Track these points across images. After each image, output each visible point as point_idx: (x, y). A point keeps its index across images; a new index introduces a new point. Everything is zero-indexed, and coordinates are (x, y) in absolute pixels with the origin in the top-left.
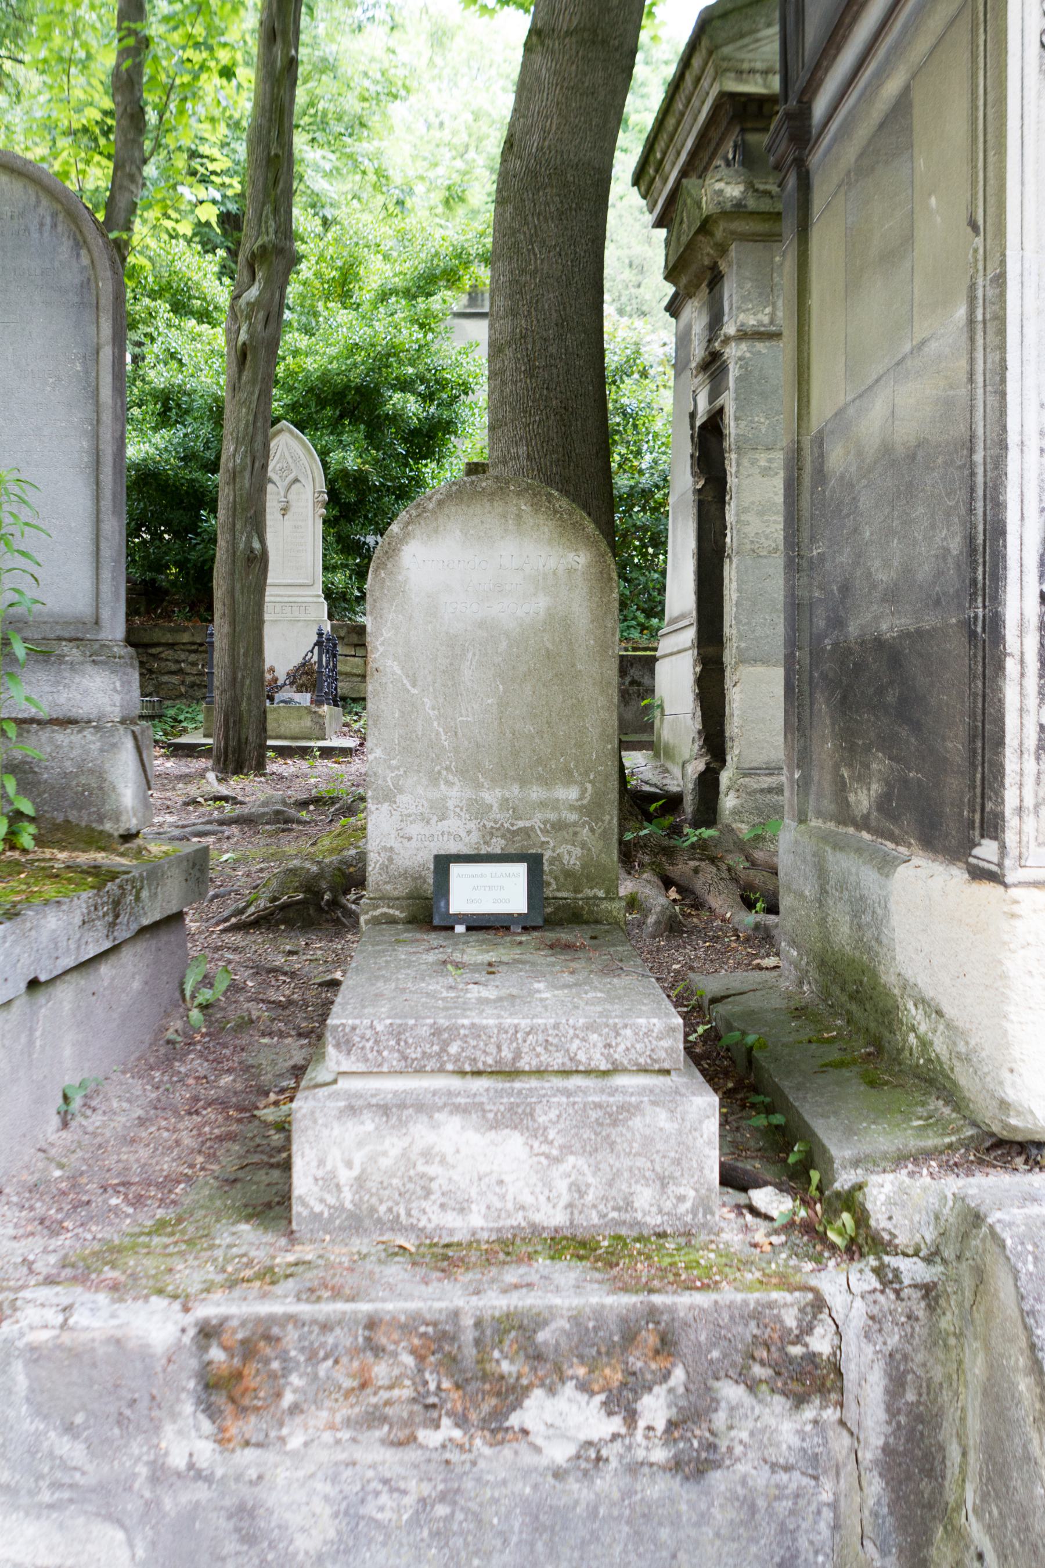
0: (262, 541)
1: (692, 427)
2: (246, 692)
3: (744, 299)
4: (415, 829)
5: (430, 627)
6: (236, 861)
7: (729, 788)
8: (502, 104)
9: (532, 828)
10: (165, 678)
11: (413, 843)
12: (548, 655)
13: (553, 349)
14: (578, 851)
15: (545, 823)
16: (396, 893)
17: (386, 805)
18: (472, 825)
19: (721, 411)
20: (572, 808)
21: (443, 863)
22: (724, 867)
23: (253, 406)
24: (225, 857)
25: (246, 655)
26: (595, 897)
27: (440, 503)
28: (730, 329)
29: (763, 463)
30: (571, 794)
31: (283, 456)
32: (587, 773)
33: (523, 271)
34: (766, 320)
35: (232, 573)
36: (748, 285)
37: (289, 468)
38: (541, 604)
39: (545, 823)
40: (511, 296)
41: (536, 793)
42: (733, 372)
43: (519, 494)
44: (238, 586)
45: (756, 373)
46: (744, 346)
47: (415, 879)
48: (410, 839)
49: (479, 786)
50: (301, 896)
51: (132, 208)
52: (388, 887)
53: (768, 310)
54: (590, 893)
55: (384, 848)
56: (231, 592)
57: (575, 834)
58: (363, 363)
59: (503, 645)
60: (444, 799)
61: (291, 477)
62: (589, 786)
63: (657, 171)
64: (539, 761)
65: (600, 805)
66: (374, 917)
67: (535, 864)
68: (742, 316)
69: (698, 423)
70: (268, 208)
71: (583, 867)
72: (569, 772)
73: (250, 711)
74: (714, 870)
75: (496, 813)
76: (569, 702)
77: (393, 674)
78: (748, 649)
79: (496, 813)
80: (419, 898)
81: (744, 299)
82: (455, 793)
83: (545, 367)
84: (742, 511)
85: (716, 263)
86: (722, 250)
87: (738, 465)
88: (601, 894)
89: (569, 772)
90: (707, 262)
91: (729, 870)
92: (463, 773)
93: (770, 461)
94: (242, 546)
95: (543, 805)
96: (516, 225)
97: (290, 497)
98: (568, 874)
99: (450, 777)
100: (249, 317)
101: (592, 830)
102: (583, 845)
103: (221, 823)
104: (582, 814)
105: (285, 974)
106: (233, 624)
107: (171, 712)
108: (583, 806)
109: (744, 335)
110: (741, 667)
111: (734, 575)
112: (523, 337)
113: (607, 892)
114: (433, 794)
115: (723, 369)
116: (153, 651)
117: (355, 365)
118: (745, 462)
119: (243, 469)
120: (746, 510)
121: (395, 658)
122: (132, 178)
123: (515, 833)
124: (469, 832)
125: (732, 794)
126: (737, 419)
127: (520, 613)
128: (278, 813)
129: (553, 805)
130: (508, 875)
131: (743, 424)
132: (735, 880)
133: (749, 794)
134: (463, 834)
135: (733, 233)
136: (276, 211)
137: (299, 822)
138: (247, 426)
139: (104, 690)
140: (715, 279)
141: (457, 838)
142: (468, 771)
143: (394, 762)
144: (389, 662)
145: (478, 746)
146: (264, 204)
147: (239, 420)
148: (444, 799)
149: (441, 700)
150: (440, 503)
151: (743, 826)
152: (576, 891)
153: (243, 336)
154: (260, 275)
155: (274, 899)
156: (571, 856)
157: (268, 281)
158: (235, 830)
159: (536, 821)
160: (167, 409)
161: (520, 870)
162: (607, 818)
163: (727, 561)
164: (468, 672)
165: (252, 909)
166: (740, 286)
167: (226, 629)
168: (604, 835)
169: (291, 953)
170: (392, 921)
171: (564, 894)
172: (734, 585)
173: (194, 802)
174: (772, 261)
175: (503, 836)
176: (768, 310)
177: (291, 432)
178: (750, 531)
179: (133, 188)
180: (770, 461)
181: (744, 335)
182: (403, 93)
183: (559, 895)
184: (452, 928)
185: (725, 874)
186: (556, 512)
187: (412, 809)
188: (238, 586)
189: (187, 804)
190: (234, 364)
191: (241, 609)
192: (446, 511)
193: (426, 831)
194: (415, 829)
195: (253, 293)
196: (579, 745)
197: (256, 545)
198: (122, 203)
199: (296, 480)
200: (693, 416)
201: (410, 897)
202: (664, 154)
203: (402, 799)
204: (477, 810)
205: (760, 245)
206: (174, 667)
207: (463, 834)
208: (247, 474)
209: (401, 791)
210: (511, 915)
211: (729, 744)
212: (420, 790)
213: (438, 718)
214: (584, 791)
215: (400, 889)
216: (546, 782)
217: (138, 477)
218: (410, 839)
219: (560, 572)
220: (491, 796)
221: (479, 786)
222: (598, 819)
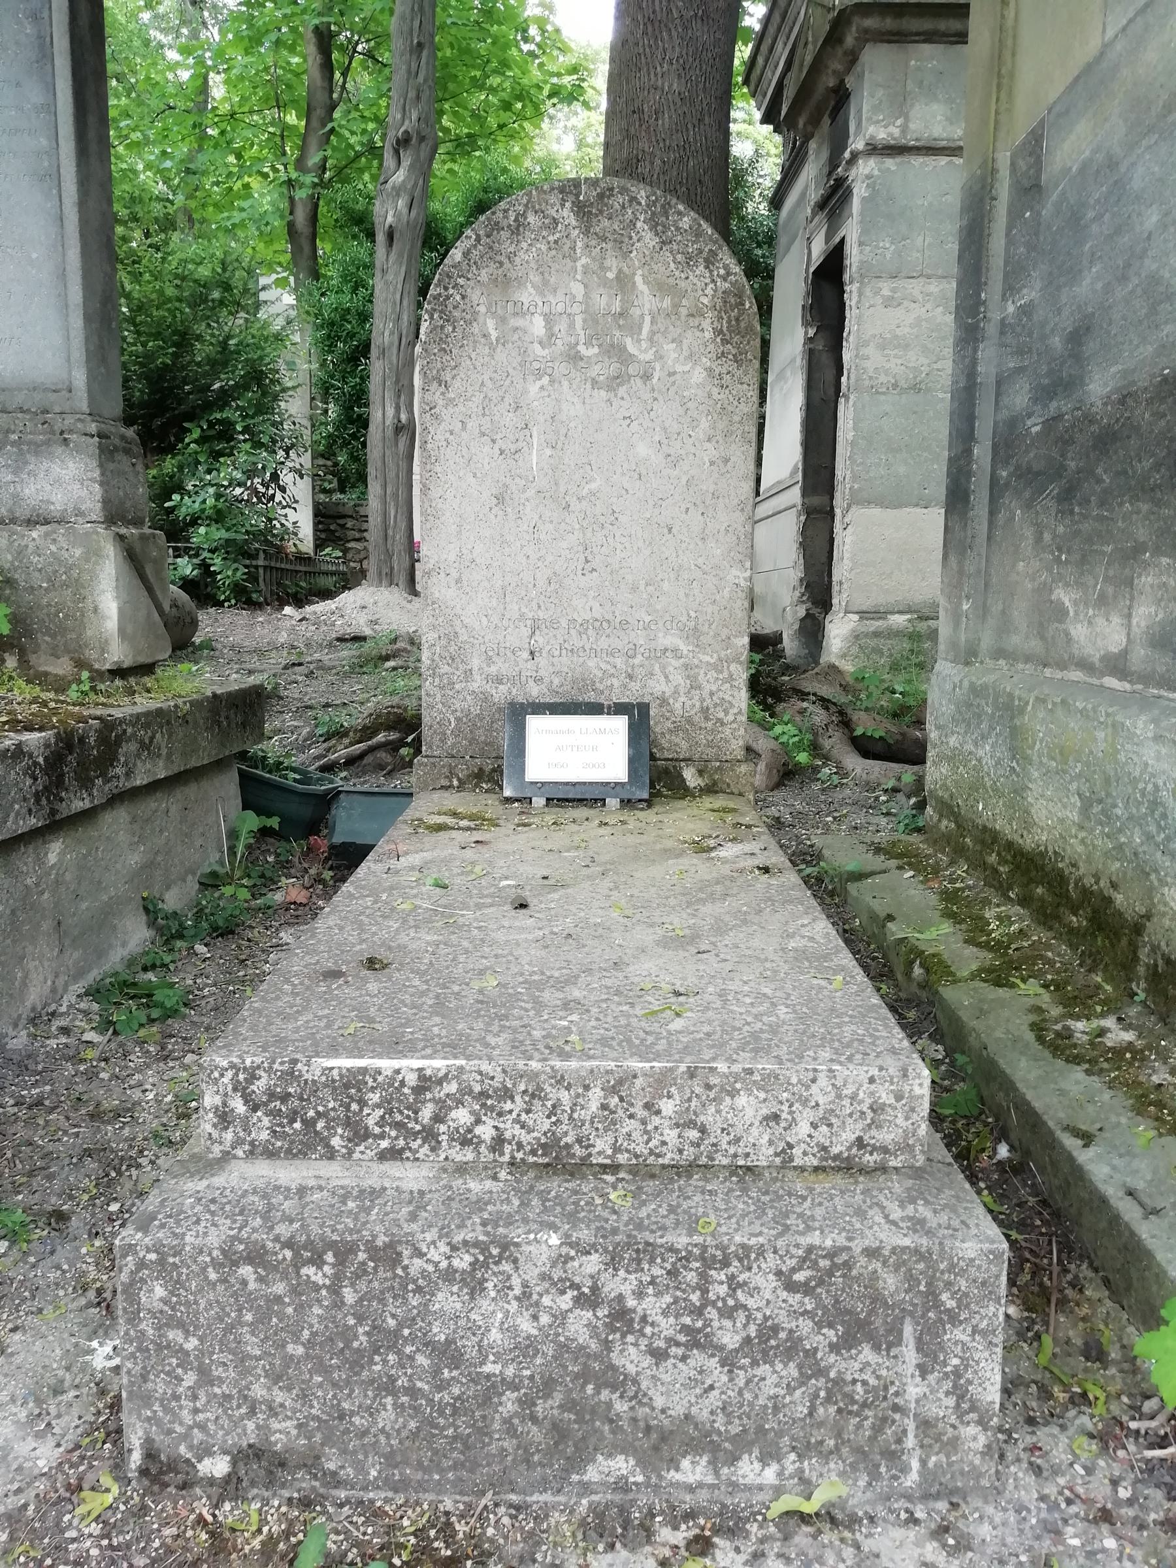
3: (876, 109)
28: (857, 144)
29: (886, 292)
34: (896, 132)
42: (859, 192)
53: (899, 122)
67: (639, 717)
68: (872, 130)
81: (876, 109)
86: (853, 59)
87: (860, 295)
90: (832, 82)
109: (875, 150)
116: (341, 522)
118: (868, 292)
120: (866, 344)
126: (861, 244)
130: (602, 732)
135: (866, 31)
139: (69, 481)
161: (619, 725)
163: (842, 400)
174: (907, 65)
176: (899, 122)
178: (869, 365)
180: (894, 290)
181: (875, 150)
197: (404, 417)
211: (835, 588)
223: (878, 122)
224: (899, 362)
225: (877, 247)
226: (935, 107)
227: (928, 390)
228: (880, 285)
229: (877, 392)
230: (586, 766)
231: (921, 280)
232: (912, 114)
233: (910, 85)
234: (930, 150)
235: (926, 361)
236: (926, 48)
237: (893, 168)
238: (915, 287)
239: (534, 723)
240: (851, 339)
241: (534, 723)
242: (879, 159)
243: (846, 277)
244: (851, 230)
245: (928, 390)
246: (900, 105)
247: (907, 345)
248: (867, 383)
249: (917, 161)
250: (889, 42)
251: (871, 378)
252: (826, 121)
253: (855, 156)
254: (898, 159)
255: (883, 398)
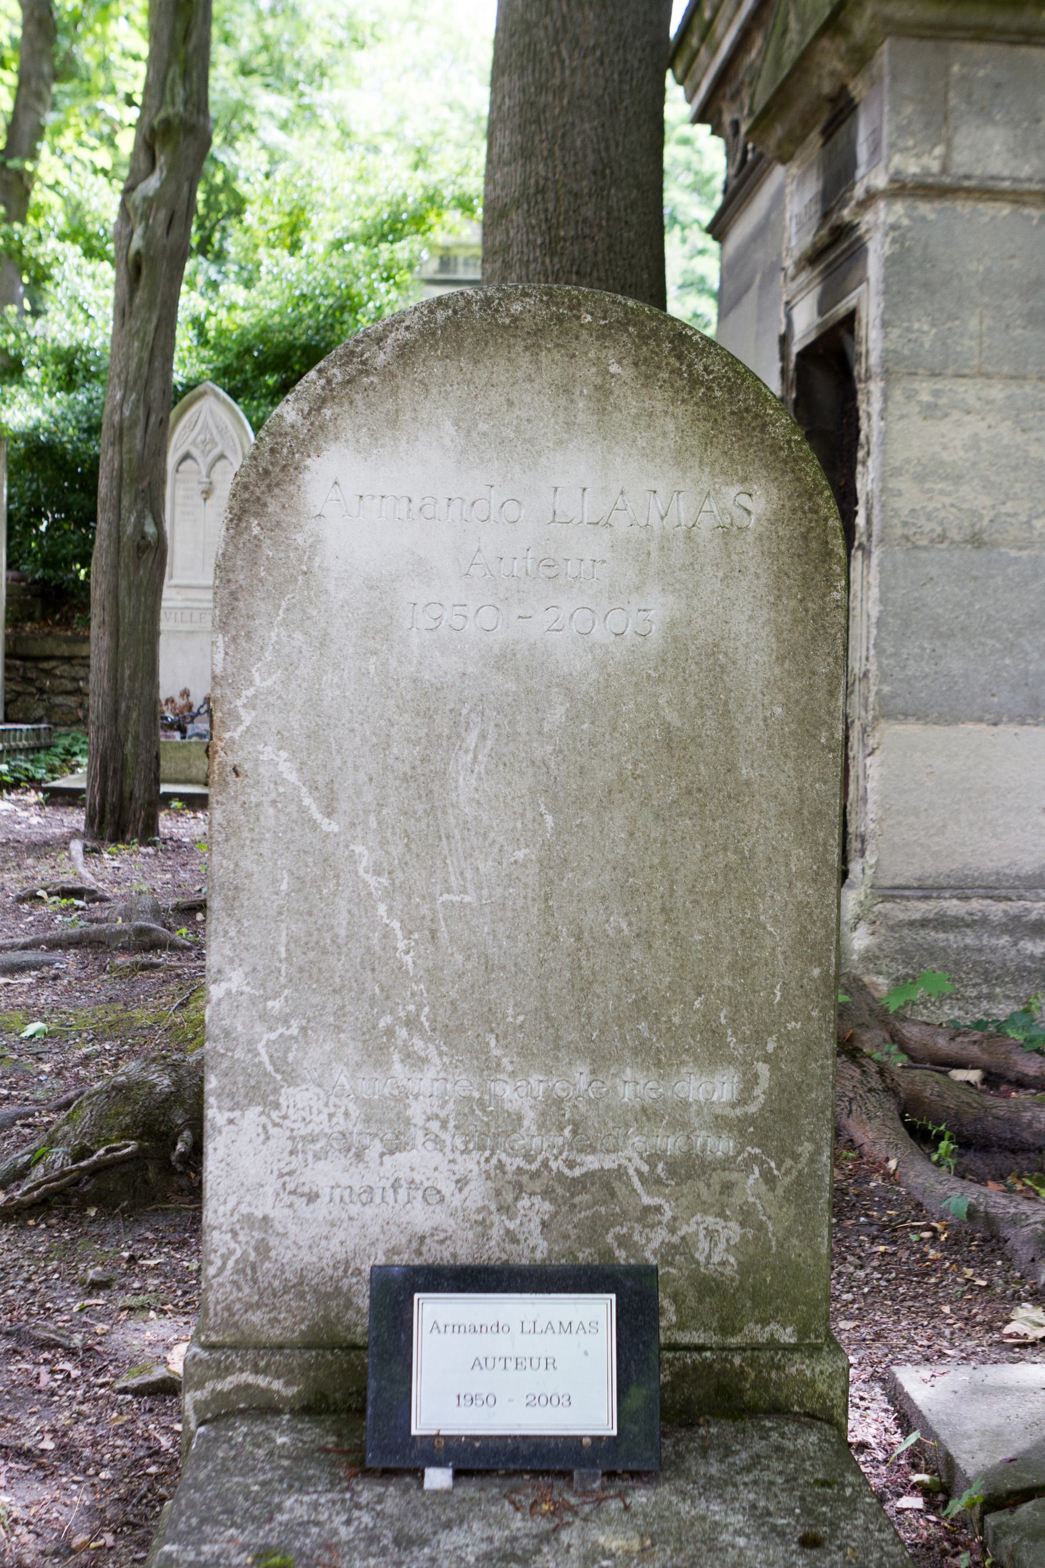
0: (159, 523)
1: (784, 356)
2: (132, 729)
3: (902, 131)
4: (325, 1174)
5: (372, 665)
6: (49, 1035)
7: (859, 919)
8: (478, 98)
9: (620, 1172)
10: (59, 700)
11: (321, 1209)
12: (669, 740)
13: (588, 211)
14: (733, 1231)
15: (652, 1160)
16: (275, 1334)
17: (253, 1113)
18: (471, 1165)
19: (850, 319)
20: (720, 1124)
21: (397, 1291)
22: (873, 1068)
23: (149, 338)
24: (31, 1029)
25: (133, 678)
26: (773, 1344)
27: (405, 353)
29: (925, 397)
30: (720, 1088)
31: (205, 426)
32: (758, 1037)
33: (542, 88)
34: (935, 166)
35: (116, 566)
36: (908, 109)
37: (213, 441)
38: (653, 612)
39: (652, 1160)
40: (522, 128)
41: (632, 1086)
42: (877, 252)
43: (603, 335)
44: (123, 584)
45: (918, 253)
46: (899, 208)
47: (323, 1298)
48: (312, 1197)
49: (488, 1067)
50: (132, 1146)
51: (39, 132)
52: (256, 1317)
53: (939, 151)
54: (761, 1334)
55: (249, 1221)
56: (114, 592)
57: (727, 1187)
58: (310, 316)
59: (558, 714)
60: (402, 1097)
61: (216, 452)
62: (763, 1069)
63: (702, 40)
64: (641, 1007)
65: (788, 1118)
66: (219, 1397)
67: (638, 1300)
68: (897, 160)
69: (796, 348)
70: (175, 71)
71: (744, 1269)
72: (713, 1035)
73: (136, 755)
74: (857, 1073)
75: (530, 1136)
76: (719, 861)
77: (278, 780)
78: (894, 695)
79: (530, 1136)
80: (332, 1346)
81: (902, 131)
82: (429, 1085)
83: (574, 239)
84: (889, 473)
85: (843, 89)
86: (861, 58)
87: (886, 398)
88: (787, 1336)
89: (713, 1035)
90: (827, 88)
91: (881, 1072)
92: (447, 1033)
93: (936, 393)
94: (129, 529)
95: (648, 1115)
96: (532, 16)
97: (214, 476)
98: (707, 1287)
99: (418, 1044)
100: (145, 217)
101: (769, 1179)
102: (746, 1216)
103: (54, 945)
104: (743, 1138)
105: (71, 1353)
106: (115, 635)
107: (65, 742)
108: (747, 1120)
109: (902, 189)
110: (883, 725)
111: (874, 577)
112: (541, 191)
113: (803, 1332)
114: (375, 1086)
115: (857, 251)
116: (45, 665)
117: (300, 319)
118: (897, 394)
119: (134, 424)
120: (896, 472)
121: (284, 740)
122: (39, 96)
123: (579, 1185)
124: (462, 1183)
125: (863, 929)
126: (885, 324)
127: (601, 634)
128: (141, 931)
129: (676, 1116)
131: (895, 333)
132: (891, 1090)
133: (892, 928)
134: (447, 1188)
135: (887, 21)
136: (186, 75)
137: (174, 947)
138: (140, 366)
140: (840, 112)
141: (433, 1196)
142: (463, 1030)
143: (275, 1005)
144: (268, 752)
145: (488, 967)
146: (169, 65)
147: (129, 358)
148: (402, 1097)
149: (397, 850)
150: (405, 353)
151: (881, 980)
152: (727, 1328)
153: (137, 243)
154: (161, 160)
155: (82, 1153)
156: (716, 1243)
157: (173, 168)
158: (68, 961)
159: (630, 1155)
160: (71, 371)
161: (598, 1311)
162: (806, 1148)
164: (466, 783)
165: (38, 1172)
166: (896, 110)
167: (106, 642)
168: (799, 1192)
169: (97, 1286)
170: (265, 1408)
171: (697, 1338)
172: (875, 592)
173: (33, 897)
175: (547, 1193)
176: (939, 151)
177: (217, 395)
178: (901, 506)
179: (40, 108)
180: (936, 393)
181: (902, 189)
182: (370, 41)
183: (685, 1338)
184: (418, 1474)
185: (875, 1082)
186: (695, 382)
187: (320, 1123)
188: (123, 584)
189: (21, 900)
190: (124, 283)
191: (128, 616)
192: (420, 372)
193: (356, 1178)
194: (325, 1174)
195: (152, 184)
196: (741, 969)
197: (150, 529)
198: (26, 127)
199: (222, 457)
200: (784, 340)
201: (310, 1343)
202: (716, 11)
203: (296, 1098)
204: (483, 1126)
205: (928, 45)
206: (70, 686)
207: (447, 1188)
208: (139, 432)
209: (292, 1078)
210: (576, 1440)
212: (341, 1076)
213: (388, 894)
214: (750, 1082)
215: (286, 1323)
216: (658, 1059)
217: (28, 450)
218: (312, 1197)
219: (704, 532)
220: (518, 1093)
221: (488, 1067)
222: (784, 1152)
223: (906, 149)
224: (947, 501)
225: (908, 330)
226: (990, 132)
227: (994, 545)
228: (916, 385)
229: (916, 547)
230: (534, 1401)
231: (979, 381)
232: (959, 140)
233: (953, 99)
234: (987, 192)
235: (988, 501)
236: (980, 50)
237: (932, 216)
238: (968, 391)
239: (430, 1310)
240: (870, 463)
241: (430, 1310)
242: (908, 202)
243: (859, 370)
244: (869, 300)
245: (994, 545)
246: (938, 122)
247: (960, 477)
248: (899, 531)
249: (963, 207)
250: (922, 38)
251: (905, 524)
252: (815, 138)
253: (871, 197)
254: (937, 205)
255: (924, 555)
